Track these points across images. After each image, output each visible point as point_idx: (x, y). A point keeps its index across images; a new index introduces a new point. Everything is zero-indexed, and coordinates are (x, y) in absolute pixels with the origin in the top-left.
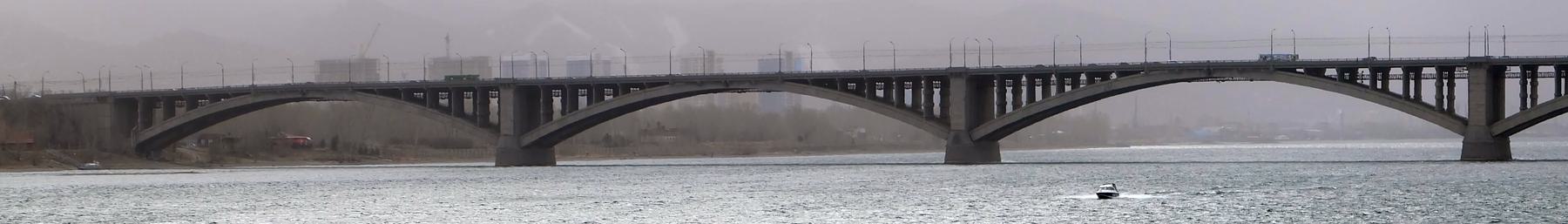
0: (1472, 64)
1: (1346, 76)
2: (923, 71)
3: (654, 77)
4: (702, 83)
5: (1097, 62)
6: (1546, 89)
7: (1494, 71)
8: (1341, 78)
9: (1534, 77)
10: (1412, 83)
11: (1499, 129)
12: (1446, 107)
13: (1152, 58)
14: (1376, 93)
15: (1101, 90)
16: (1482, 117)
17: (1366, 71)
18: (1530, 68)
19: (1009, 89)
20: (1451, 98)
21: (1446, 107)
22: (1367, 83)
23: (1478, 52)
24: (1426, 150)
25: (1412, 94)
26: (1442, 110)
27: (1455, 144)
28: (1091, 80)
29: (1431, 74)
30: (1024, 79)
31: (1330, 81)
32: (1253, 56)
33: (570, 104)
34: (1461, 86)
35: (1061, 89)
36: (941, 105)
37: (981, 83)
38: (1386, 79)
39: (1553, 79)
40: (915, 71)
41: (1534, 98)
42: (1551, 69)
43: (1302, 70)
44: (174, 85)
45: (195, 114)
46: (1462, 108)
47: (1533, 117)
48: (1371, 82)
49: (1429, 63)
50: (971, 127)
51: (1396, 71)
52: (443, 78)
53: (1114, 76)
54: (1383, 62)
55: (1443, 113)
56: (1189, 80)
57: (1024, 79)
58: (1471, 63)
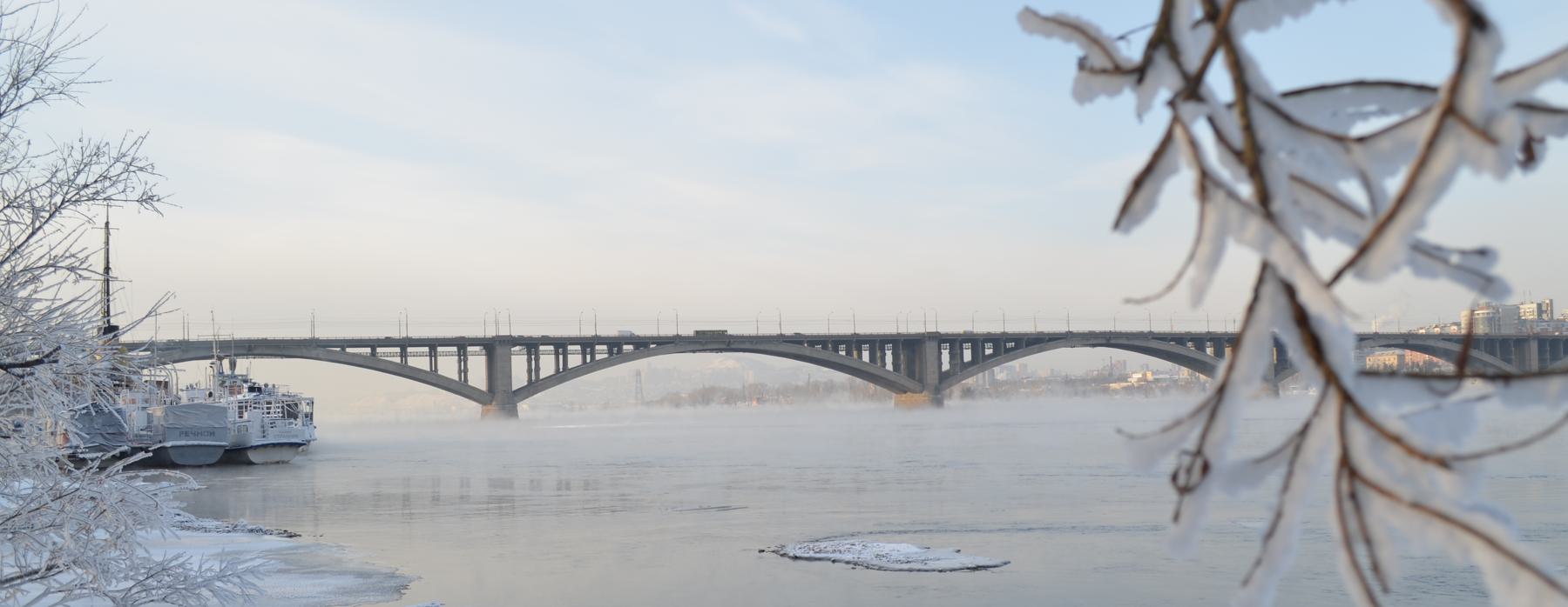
2: (878, 336)
3: (1054, 334)
4: (743, 342)
5: (802, 332)
7: (495, 348)
10: (561, 357)
15: (815, 355)
18: (532, 346)
24: (1500, 338)
32: (687, 331)
33: (955, 355)
37: (910, 347)
40: (871, 335)
41: (538, 369)
43: (652, 346)
44: (996, 329)
56: (694, 352)
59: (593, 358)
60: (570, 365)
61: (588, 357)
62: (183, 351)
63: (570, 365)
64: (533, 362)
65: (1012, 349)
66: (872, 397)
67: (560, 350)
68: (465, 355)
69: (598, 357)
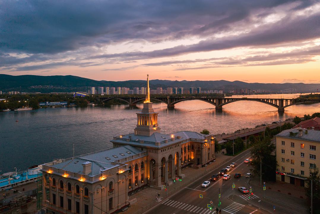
0: (279, 100)
6: (289, 103)
9: (287, 101)
11: (221, 105)
20: (277, 103)
33: (234, 100)
34: (278, 102)
38: (268, 101)
41: (287, 104)
45: (139, 100)
46: (278, 105)
49: (274, 99)
50: (218, 105)
55: (275, 106)
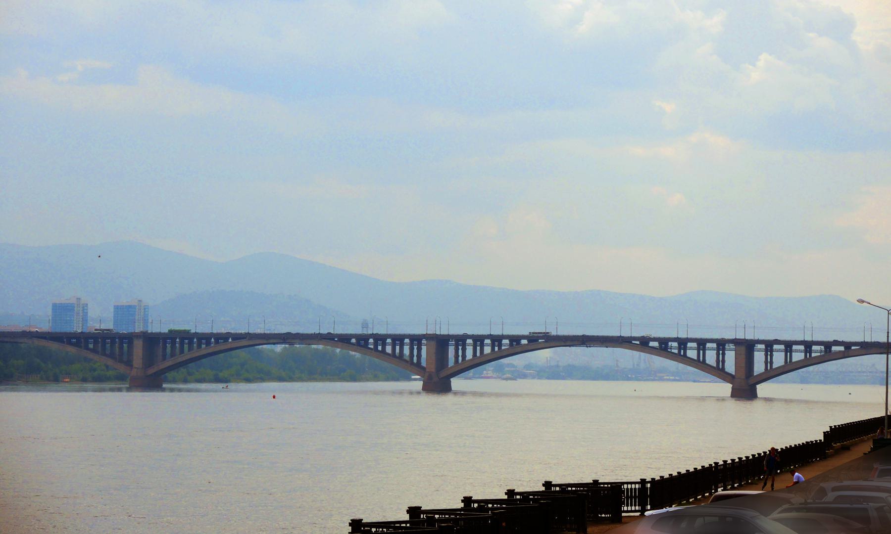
0: (736, 342)
1: (663, 347)
2: (66, 333)
4: (270, 338)
7: (746, 347)
8: (358, 344)
10: (478, 348)
11: (443, 374)
12: (721, 367)
13: (252, 331)
14: (378, 353)
16: (432, 368)
17: (675, 344)
18: (769, 345)
19: (415, 347)
20: (419, 356)
21: (721, 367)
22: (676, 351)
23: (740, 336)
25: (701, 359)
26: (412, 363)
27: (726, 388)
28: (217, 342)
29: (506, 344)
30: (195, 340)
31: (655, 350)
35: (199, 346)
36: (722, 366)
39: (454, 347)
41: (771, 363)
42: (714, 345)
47: (462, 369)
48: (678, 352)
51: (487, 341)
52: (528, 334)
53: (230, 340)
54: (498, 336)
55: (719, 372)
57: (195, 340)
58: (737, 342)
59: (500, 348)
60: (794, 360)
61: (496, 349)
62: (564, 342)
63: (794, 360)
64: (769, 357)
65: (74, 338)
66: (723, 382)
67: (496, 343)
68: (772, 351)
69: (813, 355)
